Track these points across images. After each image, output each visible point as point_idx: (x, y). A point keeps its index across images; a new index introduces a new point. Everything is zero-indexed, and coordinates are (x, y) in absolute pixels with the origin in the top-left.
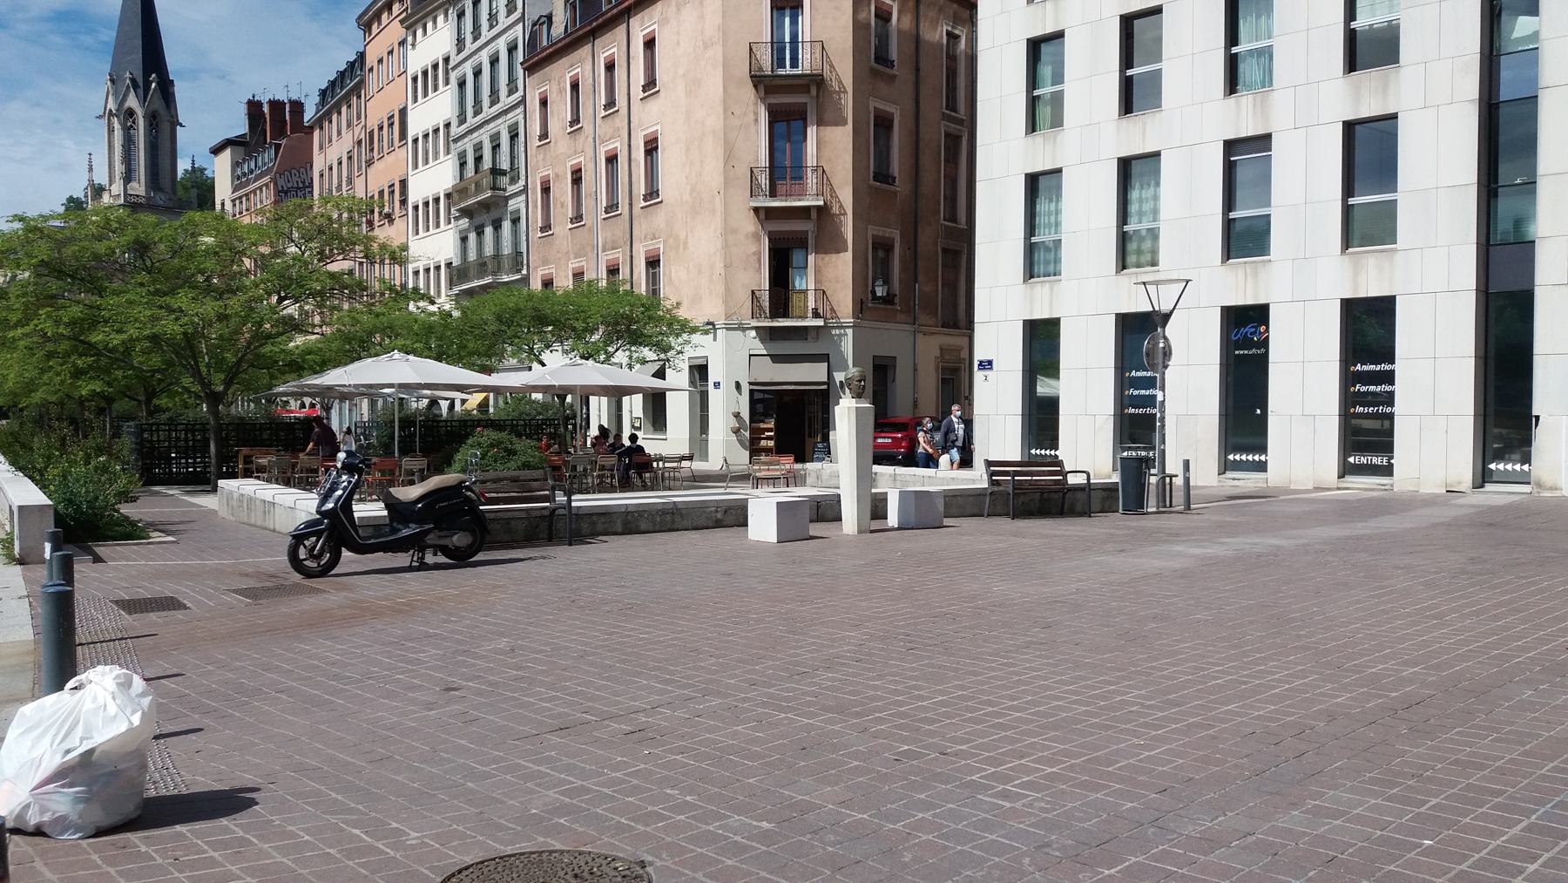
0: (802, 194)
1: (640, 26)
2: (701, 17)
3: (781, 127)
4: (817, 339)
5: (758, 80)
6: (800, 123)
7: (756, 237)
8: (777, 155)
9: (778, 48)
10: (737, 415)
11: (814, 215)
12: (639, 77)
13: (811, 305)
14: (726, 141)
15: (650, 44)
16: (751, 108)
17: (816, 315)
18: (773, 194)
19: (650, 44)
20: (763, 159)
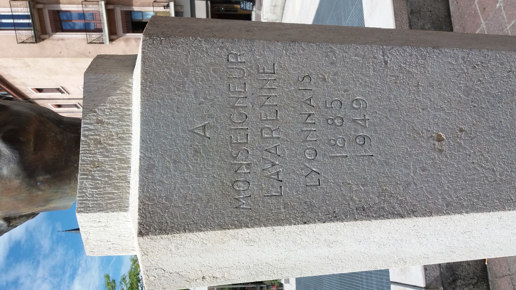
0: (99, 13)
1: (33, 95)
2: (13, 67)
3: (65, 26)
4: (181, 6)
5: (38, 38)
6: (61, 14)
7: (127, 40)
8: (77, 28)
9: (16, 27)
10: (14, 78)
11: (111, 7)
12: (58, 95)
13: (162, 9)
14: (76, 56)
15: (40, 90)
16: (55, 42)
17: (168, 6)
18: (100, 30)
19: (40, 90)
20: (82, 36)
